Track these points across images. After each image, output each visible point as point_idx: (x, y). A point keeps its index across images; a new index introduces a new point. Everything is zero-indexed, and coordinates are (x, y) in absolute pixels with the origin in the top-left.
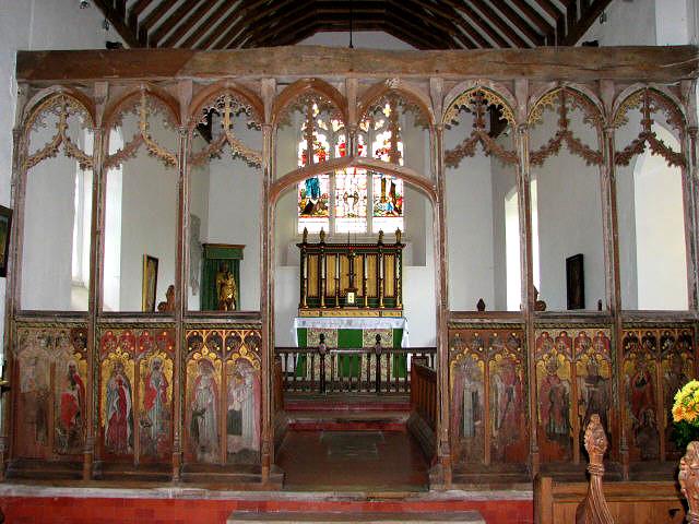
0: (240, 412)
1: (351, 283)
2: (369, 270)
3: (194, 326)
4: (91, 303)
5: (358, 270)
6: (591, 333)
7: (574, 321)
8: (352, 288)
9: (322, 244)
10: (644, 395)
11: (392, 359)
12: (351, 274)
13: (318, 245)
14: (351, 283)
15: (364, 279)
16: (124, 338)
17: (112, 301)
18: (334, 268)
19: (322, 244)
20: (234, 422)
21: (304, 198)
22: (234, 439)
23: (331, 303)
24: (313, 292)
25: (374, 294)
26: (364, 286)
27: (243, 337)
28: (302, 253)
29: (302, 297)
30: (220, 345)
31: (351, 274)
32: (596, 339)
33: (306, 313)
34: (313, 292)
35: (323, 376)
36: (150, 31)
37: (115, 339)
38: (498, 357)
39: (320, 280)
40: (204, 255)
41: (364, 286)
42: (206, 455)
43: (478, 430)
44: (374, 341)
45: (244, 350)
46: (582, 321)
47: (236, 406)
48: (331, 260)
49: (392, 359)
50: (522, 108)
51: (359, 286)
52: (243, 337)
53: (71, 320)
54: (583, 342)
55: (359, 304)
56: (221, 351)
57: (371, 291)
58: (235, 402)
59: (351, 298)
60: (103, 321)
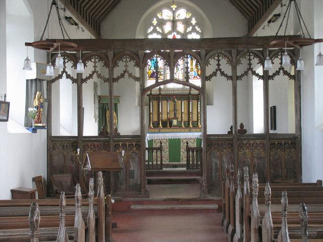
0: (134, 170)
1: (175, 114)
2: (184, 108)
3: (117, 141)
4: (79, 133)
5: (178, 107)
6: (258, 142)
7: (252, 137)
8: (175, 118)
9: (160, 94)
10: (277, 164)
11: (195, 153)
12: (175, 110)
13: (159, 95)
14: (175, 114)
15: (182, 113)
16: (91, 145)
17: (86, 133)
18: (166, 108)
19: (160, 94)
20: (131, 174)
21: (150, 69)
22: (131, 180)
23: (165, 124)
24: (155, 119)
25: (186, 120)
26: (182, 116)
27: (134, 144)
28: (150, 99)
29: (150, 122)
30: (126, 147)
31: (175, 110)
32: (260, 144)
33: (152, 130)
34: (155, 119)
35: (159, 102)
36: (88, 12)
37: (88, 146)
38: (225, 150)
39: (159, 114)
40: (99, 102)
41: (182, 116)
42: (122, 186)
43: (218, 176)
44: (159, 144)
45: (135, 149)
46: (255, 137)
47: (132, 168)
48: (164, 102)
49: (195, 153)
50: (234, 60)
51: (179, 116)
52: (134, 144)
53: (72, 139)
54: (255, 145)
55: (179, 126)
56: (126, 150)
57: (185, 118)
58: (132, 167)
59: (175, 122)
60: (84, 139)
